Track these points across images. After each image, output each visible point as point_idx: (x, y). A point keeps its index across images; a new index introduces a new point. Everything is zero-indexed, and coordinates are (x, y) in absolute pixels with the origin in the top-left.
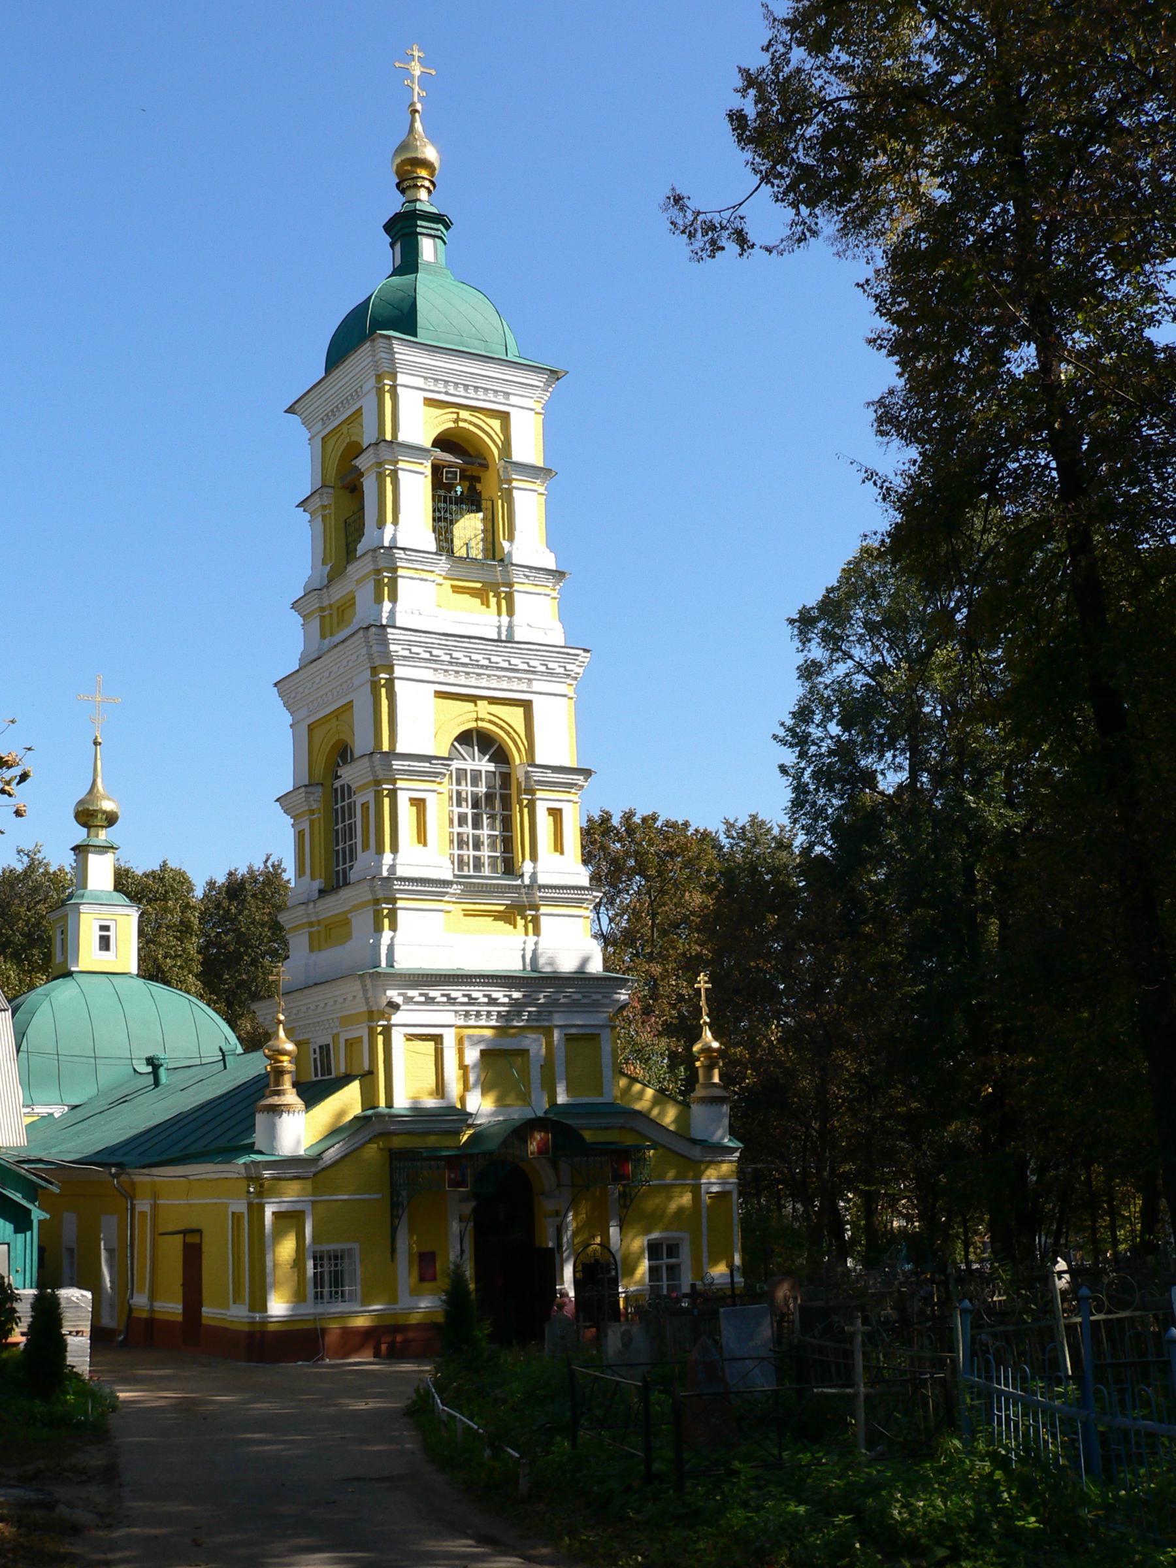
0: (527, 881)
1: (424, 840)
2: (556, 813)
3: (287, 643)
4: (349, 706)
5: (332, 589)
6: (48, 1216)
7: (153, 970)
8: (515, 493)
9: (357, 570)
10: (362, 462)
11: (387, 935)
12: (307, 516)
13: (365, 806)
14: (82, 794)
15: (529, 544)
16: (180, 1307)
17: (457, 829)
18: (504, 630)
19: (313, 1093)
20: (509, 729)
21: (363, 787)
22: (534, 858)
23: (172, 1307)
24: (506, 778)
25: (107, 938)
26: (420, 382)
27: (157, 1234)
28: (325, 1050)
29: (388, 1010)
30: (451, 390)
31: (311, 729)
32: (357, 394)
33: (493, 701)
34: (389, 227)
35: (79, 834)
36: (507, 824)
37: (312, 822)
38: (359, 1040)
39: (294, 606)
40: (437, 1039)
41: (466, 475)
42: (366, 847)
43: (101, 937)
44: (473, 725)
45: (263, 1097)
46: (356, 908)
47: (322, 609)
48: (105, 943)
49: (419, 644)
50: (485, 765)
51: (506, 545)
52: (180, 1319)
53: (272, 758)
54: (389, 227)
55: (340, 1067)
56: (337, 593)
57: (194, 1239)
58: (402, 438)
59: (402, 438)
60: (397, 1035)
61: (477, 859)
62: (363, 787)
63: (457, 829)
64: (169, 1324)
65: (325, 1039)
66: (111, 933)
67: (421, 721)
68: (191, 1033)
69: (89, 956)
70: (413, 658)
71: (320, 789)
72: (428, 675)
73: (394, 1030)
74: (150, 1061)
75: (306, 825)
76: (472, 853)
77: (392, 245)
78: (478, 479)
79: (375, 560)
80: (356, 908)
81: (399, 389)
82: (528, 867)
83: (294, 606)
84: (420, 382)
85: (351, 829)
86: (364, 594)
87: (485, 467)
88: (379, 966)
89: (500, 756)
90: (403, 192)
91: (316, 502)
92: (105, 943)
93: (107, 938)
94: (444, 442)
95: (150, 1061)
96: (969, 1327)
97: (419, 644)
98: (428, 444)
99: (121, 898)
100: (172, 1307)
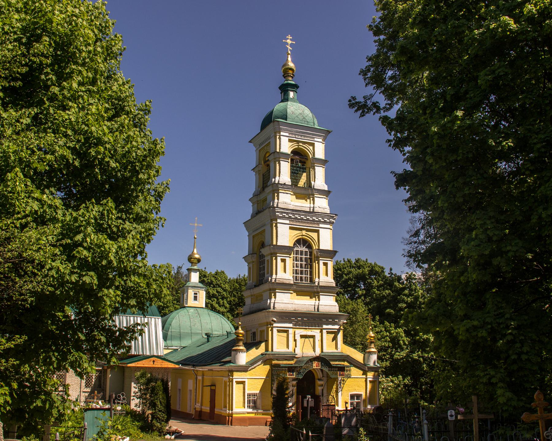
0: (316, 284)
1: (284, 271)
2: (325, 264)
3: (248, 210)
4: (264, 231)
5: (261, 195)
6: (133, 383)
7: (209, 306)
8: (316, 167)
9: (268, 190)
10: (271, 158)
11: (273, 300)
12: (254, 173)
13: (268, 261)
14: (190, 253)
15: (320, 180)
16: (209, 409)
17: (295, 268)
18: (312, 209)
19: (248, 347)
20: (312, 239)
21: (268, 255)
22: (319, 278)
23: (206, 408)
24: (311, 253)
25: (197, 298)
26: (287, 134)
27: (203, 386)
28: (254, 334)
29: (272, 322)
30: (297, 137)
31: (253, 237)
32: (269, 138)
33: (308, 230)
34: (280, 88)
35: (189, 265)
36: (311, 268)
37: (253, 265)
38: (264, 331)
39: (250, 200)
40: (287, 332)
41: (301, 161)
42: (268, 273)
43: (195, 297)
44: (301, 237)
45: (234, 346)
46: (264, 291)
47: (258, 201)
48: (195, 298)
49: (285, 213)
50: (304, 249)
51: (313, 183)
52: (209, 411)
53: (243, 246)
54: (280, 88)
55: (258, 339)
56: (262, 197)
57: (213, 388)
58: (281, 151)
59: (281, 151)
60: (275, 330)
61: (301, 278)
62: (268, 255)
63: (295, 268)
64: (205, 412)
65: (253, 330)
66: (198, 295)
67: (285, 235)
68: (220, 326)
69: (191, 302)
70: (283, 218)
71: (255, 255)
72: (288, 222)
73: (274, 329)
74: (206, 334)
75: (251, 265)
76: (300, 275)
77: (281, 93)
78: (305, 163)
79: (273, 187)
80: (264, 291)
81: (281, 137)
82: (317, 280)
83: (250, 200)
84: (287, 134)
85: (264, 267)
86: (269, 197)
87: (307, 159)
88: (270, 308)
89: (309, 246)
90: (285, 77)
91: (257, 169)
92: (195, 298)
93: (197, 298)
94: (294, 152)
95: (206, 334)
96: (265, 332)
97: (285, 213)
98: (289, 153)
99: (201, 285)
100: (206, 408)
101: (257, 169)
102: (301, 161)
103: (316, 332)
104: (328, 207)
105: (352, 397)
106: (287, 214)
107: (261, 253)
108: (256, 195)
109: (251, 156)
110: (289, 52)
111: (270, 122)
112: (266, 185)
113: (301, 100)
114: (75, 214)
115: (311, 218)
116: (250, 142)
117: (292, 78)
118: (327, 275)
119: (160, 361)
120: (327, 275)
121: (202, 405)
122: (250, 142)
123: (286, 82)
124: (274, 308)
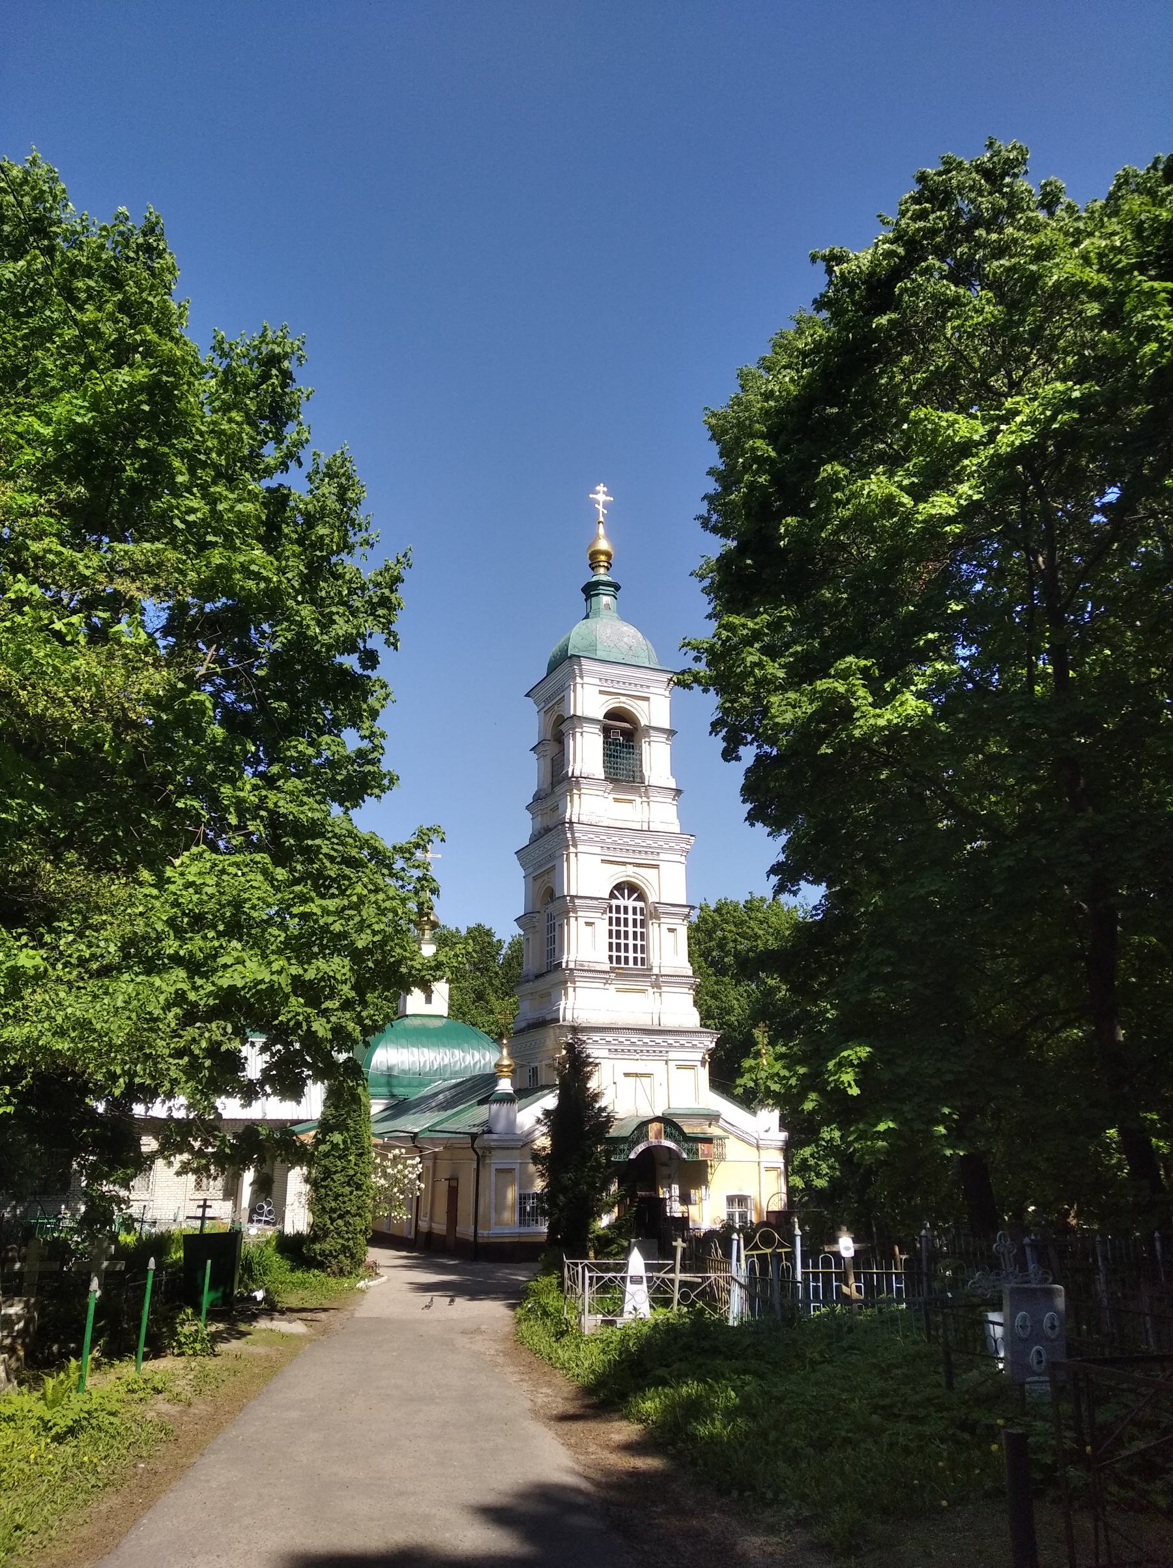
3: (522, 829)
39: (527, 808)
57: (454, 1183)
83: (527, 808)
90: (593, 569)
101: (541, 748)
102: (623, 734)
103: (654, 1066)
104: (677, 822)
105: (731, 1200)
106: (597, 834)
107: (548, 908)
108: (538, 798)
109: (530, 724)
110: (601, 519)
111: (563, 664)
112: (557, 781)
113: (626, 616)
114: (35, 650)
115: (640, 844)
116: (527, 695)
117: (608, 569)
118: (676, 952)
119: (669, 1022)
120: (676, 952)
121: (431, 1219)
122: (527, 695)
123: (594, 579)
124: (564, 1020)
